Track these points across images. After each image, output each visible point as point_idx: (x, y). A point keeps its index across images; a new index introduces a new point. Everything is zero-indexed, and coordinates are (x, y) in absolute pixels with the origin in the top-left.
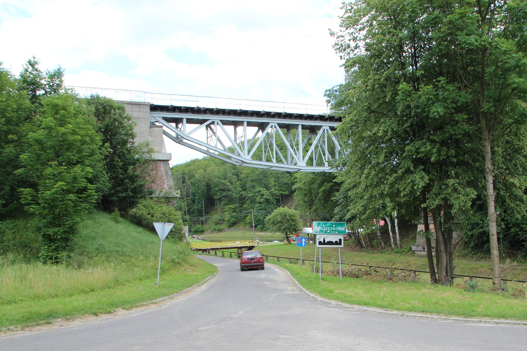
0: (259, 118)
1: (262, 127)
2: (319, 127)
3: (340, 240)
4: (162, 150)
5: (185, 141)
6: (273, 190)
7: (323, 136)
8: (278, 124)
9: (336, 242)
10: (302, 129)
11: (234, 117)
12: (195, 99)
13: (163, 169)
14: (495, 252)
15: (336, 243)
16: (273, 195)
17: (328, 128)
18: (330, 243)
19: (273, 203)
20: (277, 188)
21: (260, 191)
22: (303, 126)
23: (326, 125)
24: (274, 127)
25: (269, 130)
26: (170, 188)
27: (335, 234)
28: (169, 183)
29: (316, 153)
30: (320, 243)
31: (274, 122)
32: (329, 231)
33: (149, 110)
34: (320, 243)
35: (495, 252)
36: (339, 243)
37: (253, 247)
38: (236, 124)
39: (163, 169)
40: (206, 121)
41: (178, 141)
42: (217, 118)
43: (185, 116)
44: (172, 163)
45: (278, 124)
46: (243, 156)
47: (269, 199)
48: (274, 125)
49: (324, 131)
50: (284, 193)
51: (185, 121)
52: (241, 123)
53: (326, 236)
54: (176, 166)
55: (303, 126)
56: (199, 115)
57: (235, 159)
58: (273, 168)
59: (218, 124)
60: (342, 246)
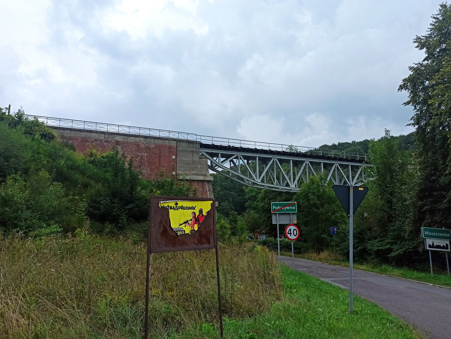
2: (303, 162)
3: (447, 245)
7: (305, 168)
8: (339, 164)
9: (443, 246)
10: (259, 160)
12: (227, 140)
14: (432, 272)
15: (443, 247)
17: (308, 162)
22: (259, 157)
23: (307, 161)
29: (267, 178)
35: (432, 272)
43: (220, 152)
46: (256, 180)
48: (275, 159)
51: (220, 155)
52: (216, 155)
55: (259, 157)
58: (292, 191)
59: (241, 159)
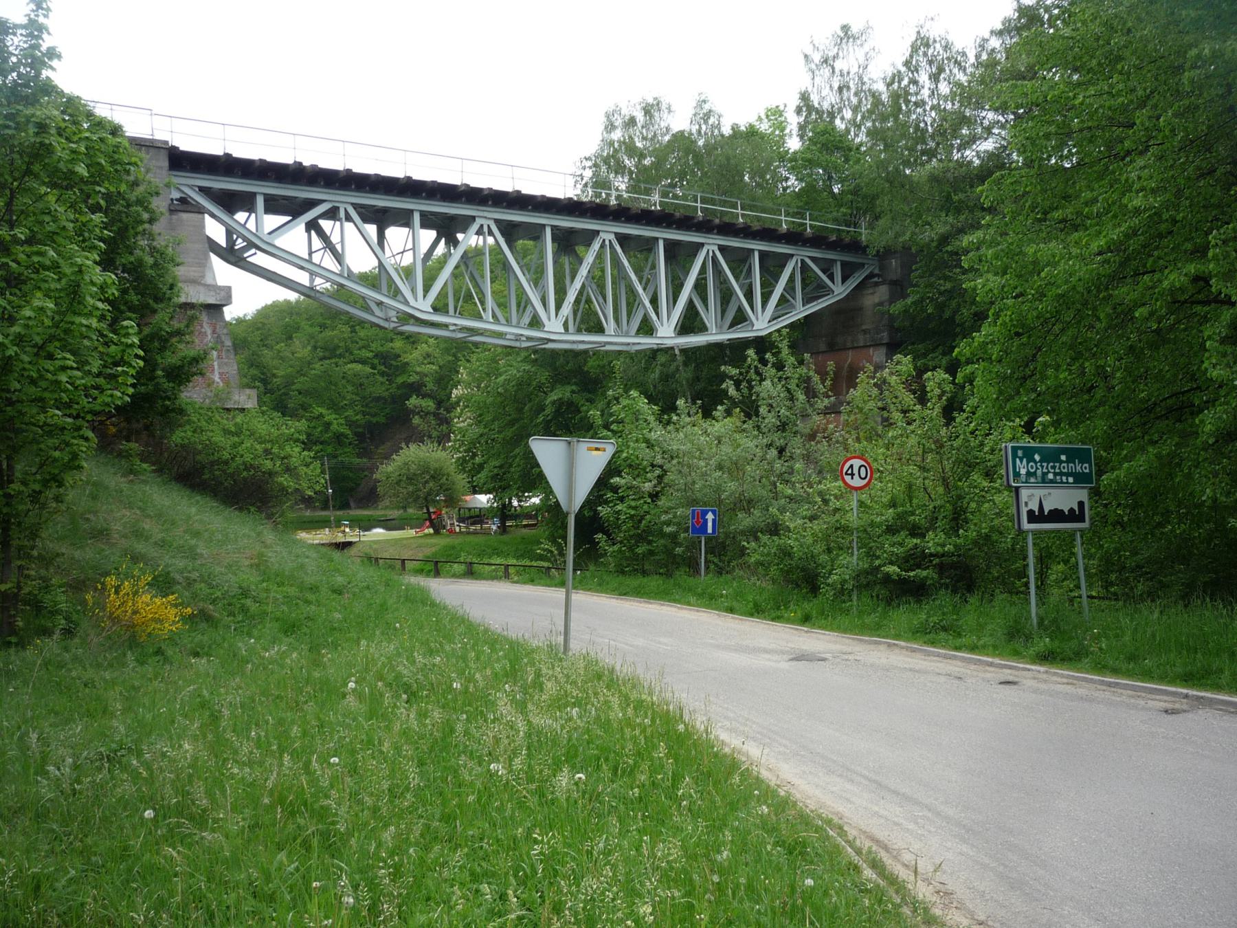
0: (443, 205)
1: (448, 228)
3: (1081, 504)
4: (203, 277)
5: (259, 259)
6: (350, 413)
8: (497, 221)
11: (385, 198)
13: (208, 329)
16: (350, 424)
17: (612, 237)
18: (1057, 515)
19: (350, 444)
20: (358, 408)
21: (321, 415)
23: (608, 232)
24: (486, 229)
25: (470, 240)
26: (227, 383)
27: (1066, 485)
28: (225, 369)
30: (1032, 517)
31: (487, 216)
32: (1051, 476)
33: (166, 164)
34: (1032, 517)
36: (1075, 516)
37: (350, 544)
38: (382, 219)
39: (208, 329)
40: (312, 204)
41: (232, 259)
42: (346, 200)
44: (230, 313)
45: (497, 221)
47: (342, 434)
48: (485, 222)
49: (603, 246)
50: (374, 420)
53: (1045, 491)
54: (240, 321)
56: (298, 188)
57: (383, 310)
59: (348, 218)
60: (1086, 525)
